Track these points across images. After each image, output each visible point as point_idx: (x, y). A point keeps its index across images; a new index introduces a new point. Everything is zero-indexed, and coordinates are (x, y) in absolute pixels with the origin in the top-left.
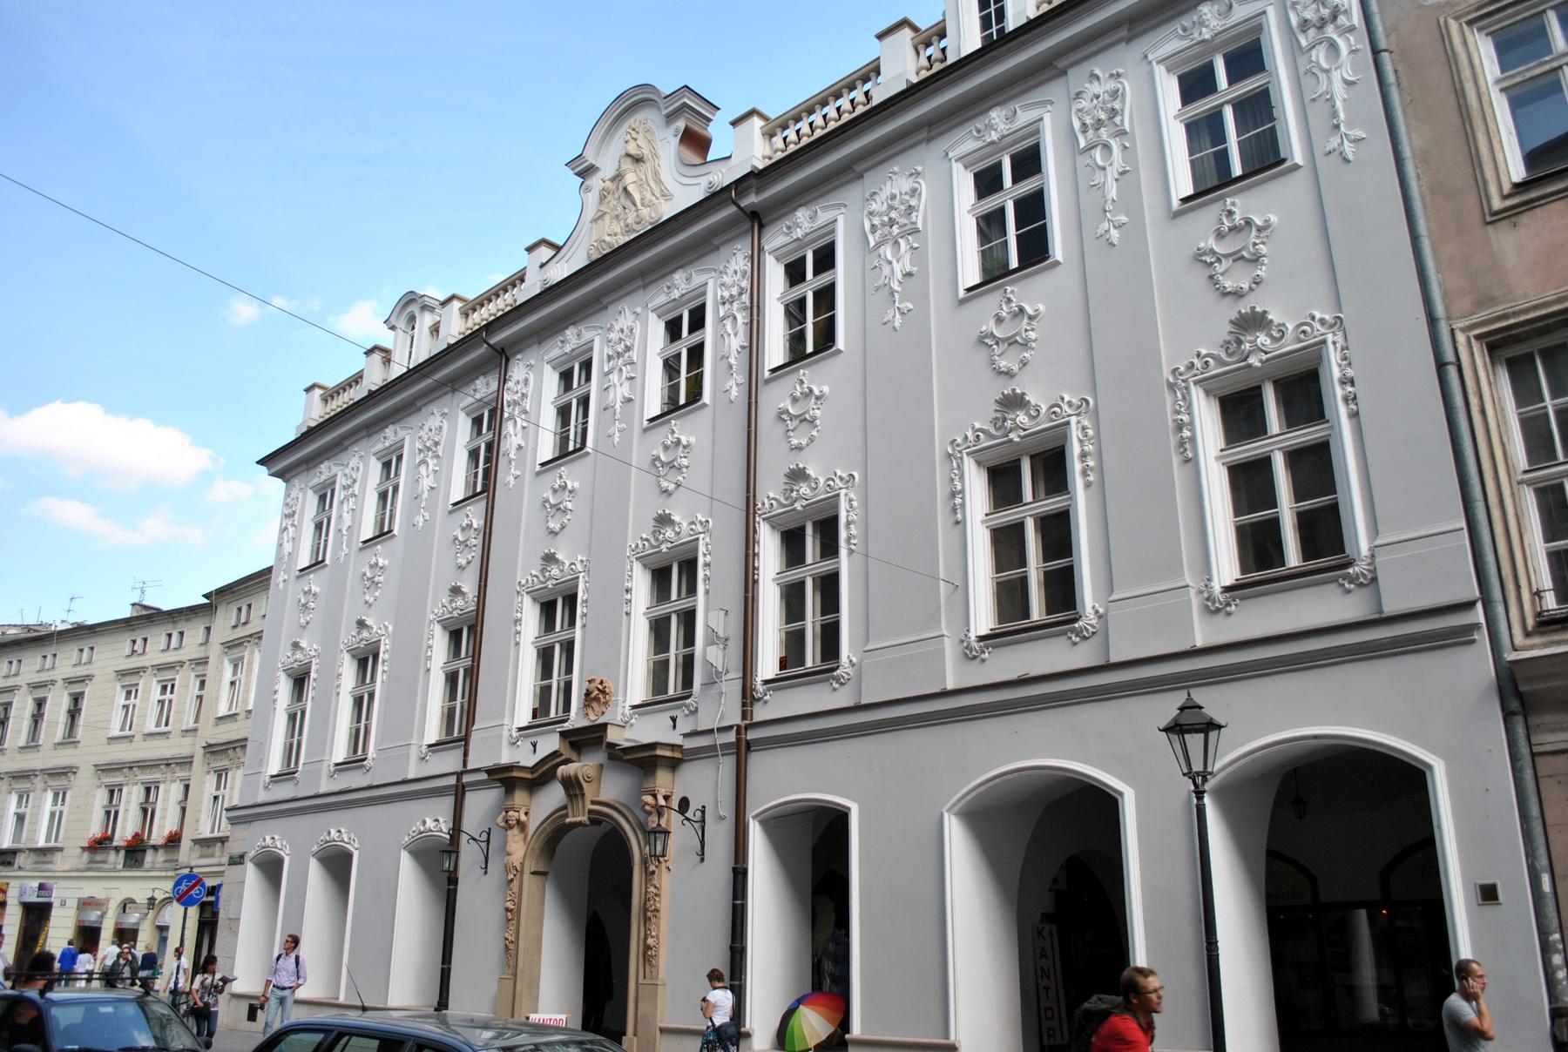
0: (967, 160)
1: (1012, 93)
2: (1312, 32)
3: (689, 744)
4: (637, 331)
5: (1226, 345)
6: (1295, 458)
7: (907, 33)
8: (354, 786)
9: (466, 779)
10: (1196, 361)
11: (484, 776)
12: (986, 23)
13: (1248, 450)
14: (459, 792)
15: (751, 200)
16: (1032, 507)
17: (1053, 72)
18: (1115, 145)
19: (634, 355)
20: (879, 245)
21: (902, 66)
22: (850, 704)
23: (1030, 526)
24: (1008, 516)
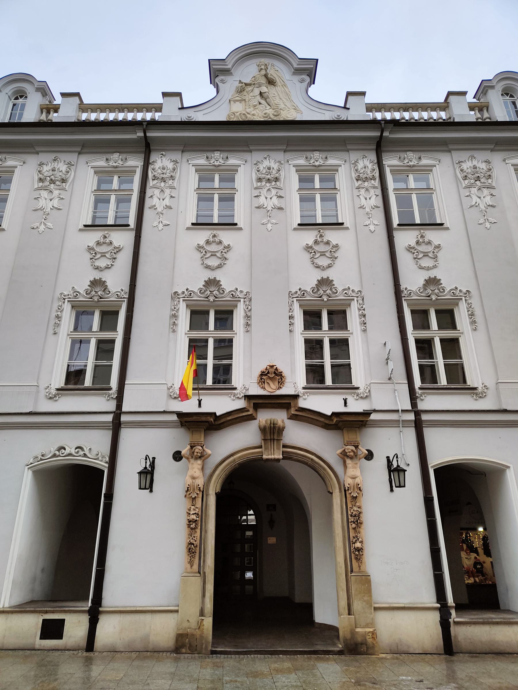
2: (360, 182)
3: (373, 417)
4: (458, 171)
5: (86, 290)
7: (77, 98)
10: (186, 292)
11: (175, 418)
13: (313, 334)
14: (116, 427)
17: (33, 151)
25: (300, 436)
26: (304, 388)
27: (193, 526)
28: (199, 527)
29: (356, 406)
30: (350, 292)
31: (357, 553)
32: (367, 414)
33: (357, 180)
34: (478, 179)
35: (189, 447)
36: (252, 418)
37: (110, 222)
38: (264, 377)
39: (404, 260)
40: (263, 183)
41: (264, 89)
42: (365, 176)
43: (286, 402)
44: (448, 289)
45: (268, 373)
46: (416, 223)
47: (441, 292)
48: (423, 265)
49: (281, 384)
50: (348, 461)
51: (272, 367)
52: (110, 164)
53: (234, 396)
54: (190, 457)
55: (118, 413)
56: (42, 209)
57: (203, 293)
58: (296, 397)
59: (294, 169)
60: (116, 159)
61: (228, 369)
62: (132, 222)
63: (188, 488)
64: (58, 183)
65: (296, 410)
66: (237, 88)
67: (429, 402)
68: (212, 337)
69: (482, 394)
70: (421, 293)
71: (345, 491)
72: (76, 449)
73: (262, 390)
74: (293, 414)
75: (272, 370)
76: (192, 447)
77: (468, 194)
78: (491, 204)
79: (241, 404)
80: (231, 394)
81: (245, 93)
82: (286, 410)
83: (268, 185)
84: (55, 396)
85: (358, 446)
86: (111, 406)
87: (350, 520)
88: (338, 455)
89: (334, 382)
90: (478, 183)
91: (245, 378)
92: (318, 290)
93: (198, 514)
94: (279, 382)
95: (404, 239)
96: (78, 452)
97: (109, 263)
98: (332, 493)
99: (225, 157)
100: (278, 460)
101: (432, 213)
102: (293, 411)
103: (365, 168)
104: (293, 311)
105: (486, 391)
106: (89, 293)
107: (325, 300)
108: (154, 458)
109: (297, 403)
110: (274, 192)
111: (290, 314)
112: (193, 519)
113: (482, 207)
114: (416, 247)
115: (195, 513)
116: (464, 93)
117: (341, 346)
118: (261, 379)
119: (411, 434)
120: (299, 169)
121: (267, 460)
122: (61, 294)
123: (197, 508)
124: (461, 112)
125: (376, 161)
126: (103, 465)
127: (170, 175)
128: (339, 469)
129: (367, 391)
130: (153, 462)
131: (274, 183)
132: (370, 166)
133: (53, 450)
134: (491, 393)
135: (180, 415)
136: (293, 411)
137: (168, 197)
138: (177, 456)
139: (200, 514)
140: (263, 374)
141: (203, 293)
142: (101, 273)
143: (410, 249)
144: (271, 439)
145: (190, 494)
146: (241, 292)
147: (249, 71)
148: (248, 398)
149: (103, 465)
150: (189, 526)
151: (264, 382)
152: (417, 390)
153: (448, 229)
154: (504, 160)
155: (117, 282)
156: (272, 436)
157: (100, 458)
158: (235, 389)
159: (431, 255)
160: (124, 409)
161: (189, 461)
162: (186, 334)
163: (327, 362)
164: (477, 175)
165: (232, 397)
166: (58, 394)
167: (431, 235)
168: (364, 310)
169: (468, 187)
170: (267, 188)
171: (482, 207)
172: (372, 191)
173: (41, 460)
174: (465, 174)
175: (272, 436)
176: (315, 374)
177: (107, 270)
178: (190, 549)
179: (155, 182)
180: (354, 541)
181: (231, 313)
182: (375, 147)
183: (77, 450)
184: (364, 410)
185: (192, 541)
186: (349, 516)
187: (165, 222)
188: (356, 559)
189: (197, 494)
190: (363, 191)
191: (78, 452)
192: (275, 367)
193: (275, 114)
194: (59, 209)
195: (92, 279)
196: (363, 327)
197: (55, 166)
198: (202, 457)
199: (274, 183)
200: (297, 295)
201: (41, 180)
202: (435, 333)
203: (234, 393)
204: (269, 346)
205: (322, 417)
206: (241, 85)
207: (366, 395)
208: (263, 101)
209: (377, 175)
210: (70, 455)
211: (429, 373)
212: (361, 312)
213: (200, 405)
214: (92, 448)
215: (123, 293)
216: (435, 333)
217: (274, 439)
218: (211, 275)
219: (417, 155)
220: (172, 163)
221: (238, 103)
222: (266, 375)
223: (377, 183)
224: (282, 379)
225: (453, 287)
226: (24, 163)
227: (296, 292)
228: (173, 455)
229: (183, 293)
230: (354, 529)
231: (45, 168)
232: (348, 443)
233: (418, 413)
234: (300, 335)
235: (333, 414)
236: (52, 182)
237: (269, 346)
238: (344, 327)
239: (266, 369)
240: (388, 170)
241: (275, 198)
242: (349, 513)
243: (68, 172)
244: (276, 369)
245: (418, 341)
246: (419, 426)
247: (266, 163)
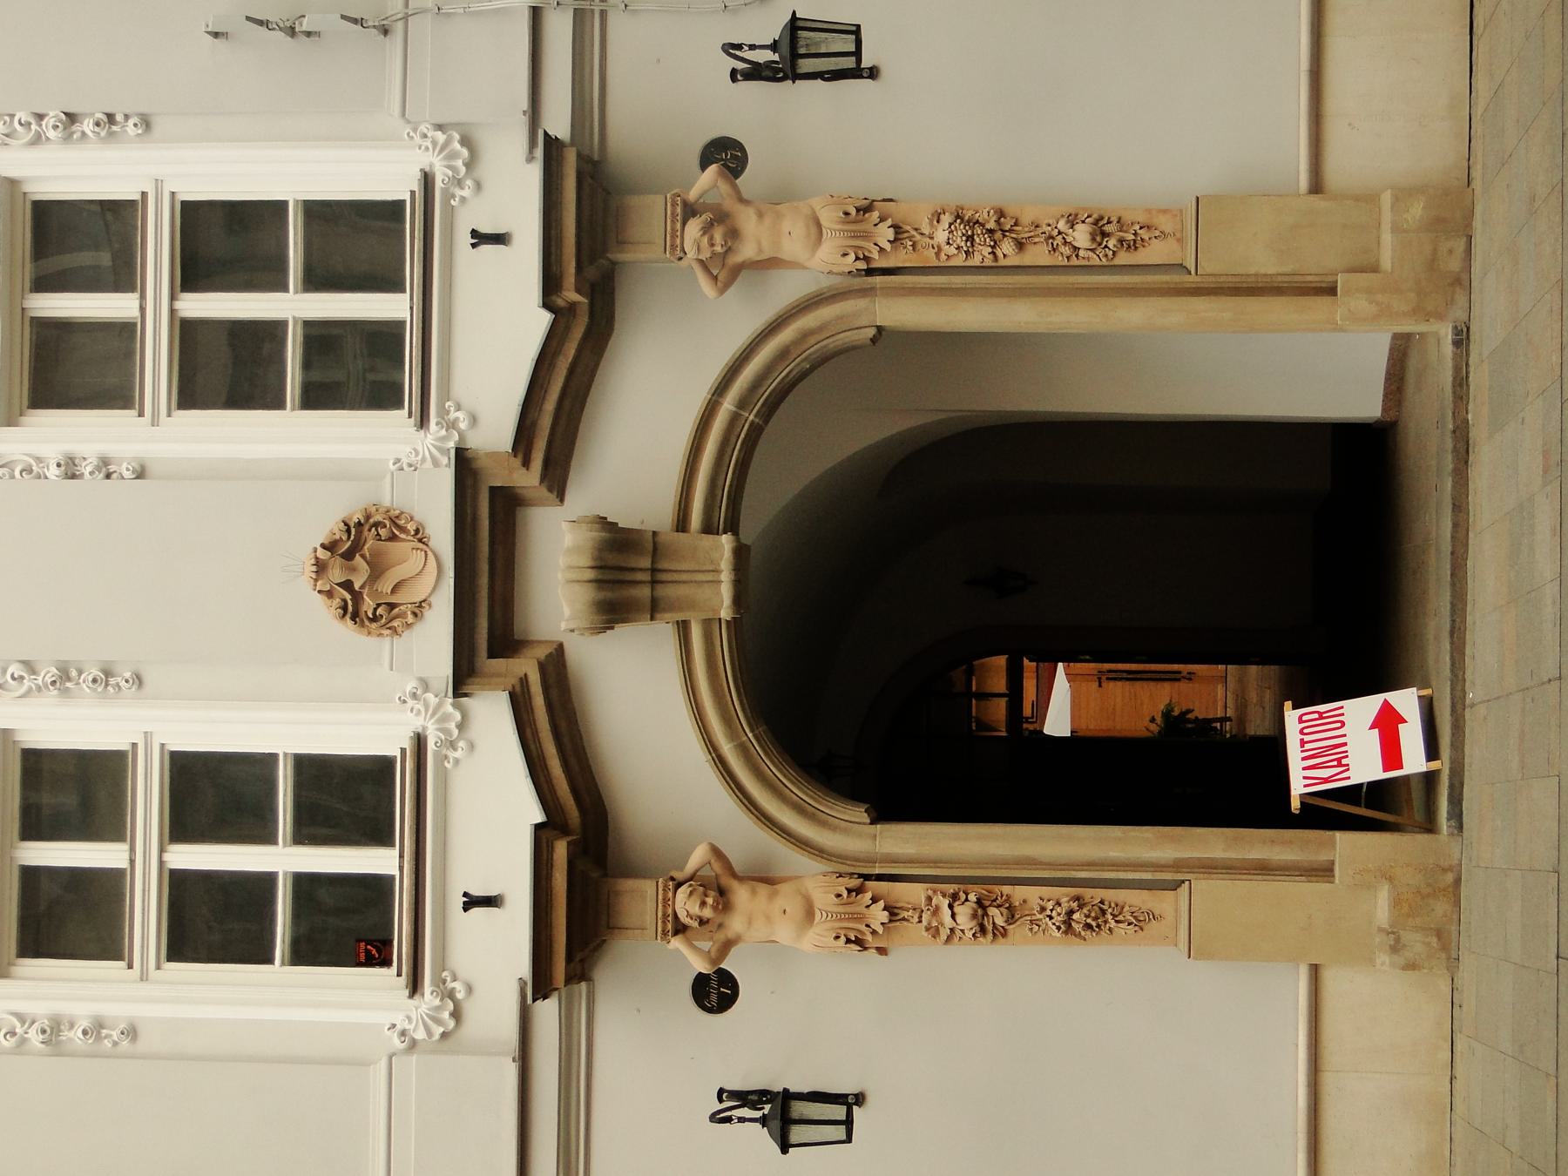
3: (558, 123)
11: (547, 1012)
27: (997, 916)
28: (1006, 889)
29: (513, 194)
31: (1112, 243)
35: (676, 943)
36: (556, 667)
43: (490, 521)
49: (403, 529)
50: (747, 251)
51: (321, 567)
53: (453, 745)
54: (726, 881)
58: (464, 463)
63: (848, 941)
65: (526, 463)
68: (173, 298)
71: (870, 272)
73: (428, 613)
74: (543, 478)
76: (680, 929)
82: (522, 513)
85: (685, 204)
87: (989, 262)
88: (722, 291)
91: (374, 696)
93: (955, 897)
94: (393, 538)
98: (880, 329)
100: (740, 553)
104: (39, 460)
109: (494, 455)
112: (974, 916)
115: (951, 907)
118: (375, 619)
121: (738, 601)
123: (930, 899)
128: (787, 289)
129: (441, 137)
136: (528, 479)
139: (951, 888)
140: (352, 612)
144: (654, 582)
145: (874, 932)
148: (464, 677)
150: (1000, 933)
151: (392, 606)
156: (640, 576)
165: (466, 193)
168: (40, 117)
175: (640, 576)
178: (1088, 926)
180: (1066, 250)
185: (1058, 919)
186: (970, 263)
188: (1133, 246)
189: (874, 900)
192: (323, 554)
196: (130, 129)
198: (717, 888)
205: (557, 353)
207: (457, 146)
212: (52, 134)
217: (654, 570)
222: (357, 597)
224: (376, 525)
228: (710, 1010)
230: (1020, 246)
232: (673, 247)
234: (144, 993)
239: (329, 594)
242: (960, 261)
244: (330, 547)
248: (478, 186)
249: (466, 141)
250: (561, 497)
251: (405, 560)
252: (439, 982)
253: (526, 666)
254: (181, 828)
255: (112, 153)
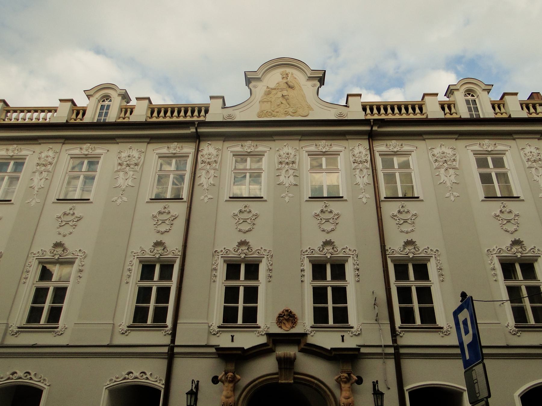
0: (235, 153)
1: (498, 137)
2: (530, 163)
3: (363, 350)
4: (142, 158)
6: (246, 289)
8: (40, 343)
9: (176, 350)
10: (224, 251)
12: (100, 115)
13: (233, 283)
14: (171, 356)
15: (201, 130)
16: (155, 284)
18: (212, 172)
19: (295, 166)
20: (118, 171)
21: (62, 115)
22: (204, 344)
23: (242, 290)
24: (233, 283)
25: (266, 367)
26: (312, 327)
29: (351, 343)
30: (348, 250)
32: (357, 350)
33: (354, 163)
34: (446, 161)
35: (224, 373)
37: (325, 195)
38: (281, 319)
39: (389, 225)
40: (283, 165)
41: (285, 93)
42: (360, 159)
43: (297, 339)
44: (339, 249)
45: (284, 315)
46: (324, 196)
47: (524, 250)
48: (405, 230)
51: (287, 311)
52: (170, 151)
55: (172, 346)
56: (119, 187)
57: (236, 251)
58: (305, 335)
59: (472, 153)
60: (174, 148)
61: (431, 311)
62: (185, 195)
64: (132, 166)
65: (305, 345)
66: (266, 91)
67: (408, 339)
69: (447, 332)
70: (401, 251)
72: (25, 373)
75: (286, 313)
77: (437, 174)
78: (455, 182)
79: (263, 340)
80: (54, 331)
81: (271, 95)
83: (287, 166)
84: (126, 332)
86: (167, 340)
89: (422, 322)
90: (445, 164)
91: (267, 320)
92: (323, 249)
94: (292, 323)
95: (390, 209)
96: (26, 376)
97: (168, 228)
99: (255, 145)
101: (509, 188)
102: (302, 346)
103: (360, 153)
105: (449, 330)
106: (152, 252)
107: (329, 257)
108: (198, 382)
110: (291, 172)
111: (302, 268)
113: (448, 184)
114: (398, 215)
116: (437, 95)
117: (340, 294)
119: (391, 364)
120: (475, 153)
122: (132, 252)
124: (433, 111)
125: (368, 148)
126: (160, 385)
127: (214, 160)
128: (337, 392)
129: (359, 330)
130: (198, 384)
131: (291, 165)
132: (364, 152)
133: (8, 373)
134: (68, 333)
135: (218, 349)
136: (302, 346)
137: (213, 176)
138: (215, 380)
140: (280, 316)
141: (236, 251)
142: (162, 236)
143: (393, 216)
146: (265, 250)
147: (274, 78)
148: (269, 335)
149: (160, 385)
152: (397, 329)
153: (12, 204)
154: (466, 147)
155: (174, 244)
157: (42, 381)
158: (259, 327)
159: (409, 221)
160: (177, 343)
161: (224, 384)
162: (223, 283)
163: (416, 305)
164: (444, 159)
166: (128, 330)
167: (409, 205)
169: (437, 168)
170: (286, 169)
171: (448, 184)
172: (365, 171)
173: (115, 381)
174: (435, 158)
176: (320, 316)
177: (166, 233)
179: (203, 165)
181: (425, 266)
182: (367, 137)
183: (141, 375)
184: (357, 345)
187: (210, 196)
190: (442, 171)
191: (26, 376)
193: (293, 111)
194: (296, 185)
195: (239, 241)
197: (130, 153)
199: (291, 165)
200: (307, 253)
201: (120, 164)
202: (413, 283)
203: (259, 331)
204: (284, 293)
206: (268, 89)
208: (284, 102)
209: (369, 159)
210: (136, 378)
211: (407, 316)
213: (232, 341)
214: (151, 373)
215: (177, 251)
216: (413, 283)
218: (328, 237)
219: (255, 143)
220: (216, 151)
221: (266, 103)
222: (283, 317)
223: (368, 165)
225: (532, 247)
226: (108, 151)
227: (307, 251)
229: (222, 251)
231: (123, 155)
233: (397, 348)
234: (308, 285)
235: (333, 349)
236: (128, 165)
237: (284, 293)
238: (256, 278)
239: (283, 312)
240: (377, 155)
241: (292, 177)
243: (139, 158)
245: (399, 289)
246: (398, 357)
247: (286, 150)
248: (443, 337)
249: (359, 334)
250: (299, 351)
251: (288, 325)
252: (219, 331)
253: (271, 346)
254: (418, 289)
255: (437, 276)
